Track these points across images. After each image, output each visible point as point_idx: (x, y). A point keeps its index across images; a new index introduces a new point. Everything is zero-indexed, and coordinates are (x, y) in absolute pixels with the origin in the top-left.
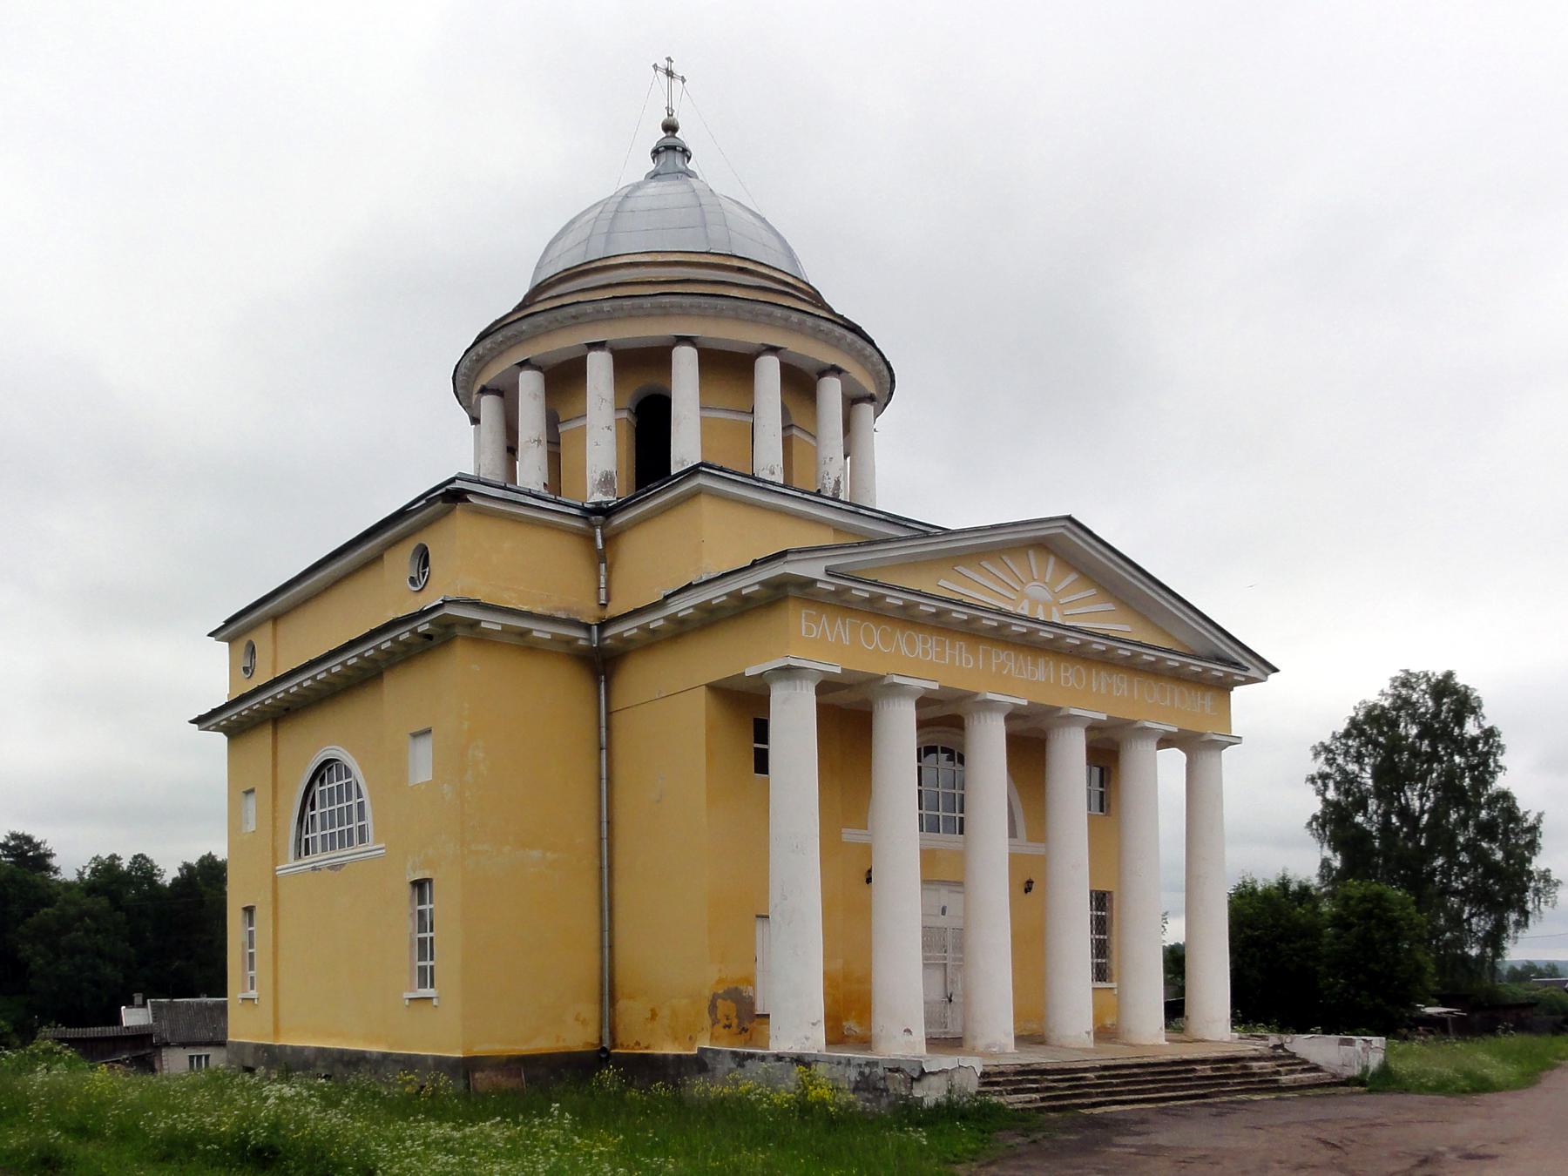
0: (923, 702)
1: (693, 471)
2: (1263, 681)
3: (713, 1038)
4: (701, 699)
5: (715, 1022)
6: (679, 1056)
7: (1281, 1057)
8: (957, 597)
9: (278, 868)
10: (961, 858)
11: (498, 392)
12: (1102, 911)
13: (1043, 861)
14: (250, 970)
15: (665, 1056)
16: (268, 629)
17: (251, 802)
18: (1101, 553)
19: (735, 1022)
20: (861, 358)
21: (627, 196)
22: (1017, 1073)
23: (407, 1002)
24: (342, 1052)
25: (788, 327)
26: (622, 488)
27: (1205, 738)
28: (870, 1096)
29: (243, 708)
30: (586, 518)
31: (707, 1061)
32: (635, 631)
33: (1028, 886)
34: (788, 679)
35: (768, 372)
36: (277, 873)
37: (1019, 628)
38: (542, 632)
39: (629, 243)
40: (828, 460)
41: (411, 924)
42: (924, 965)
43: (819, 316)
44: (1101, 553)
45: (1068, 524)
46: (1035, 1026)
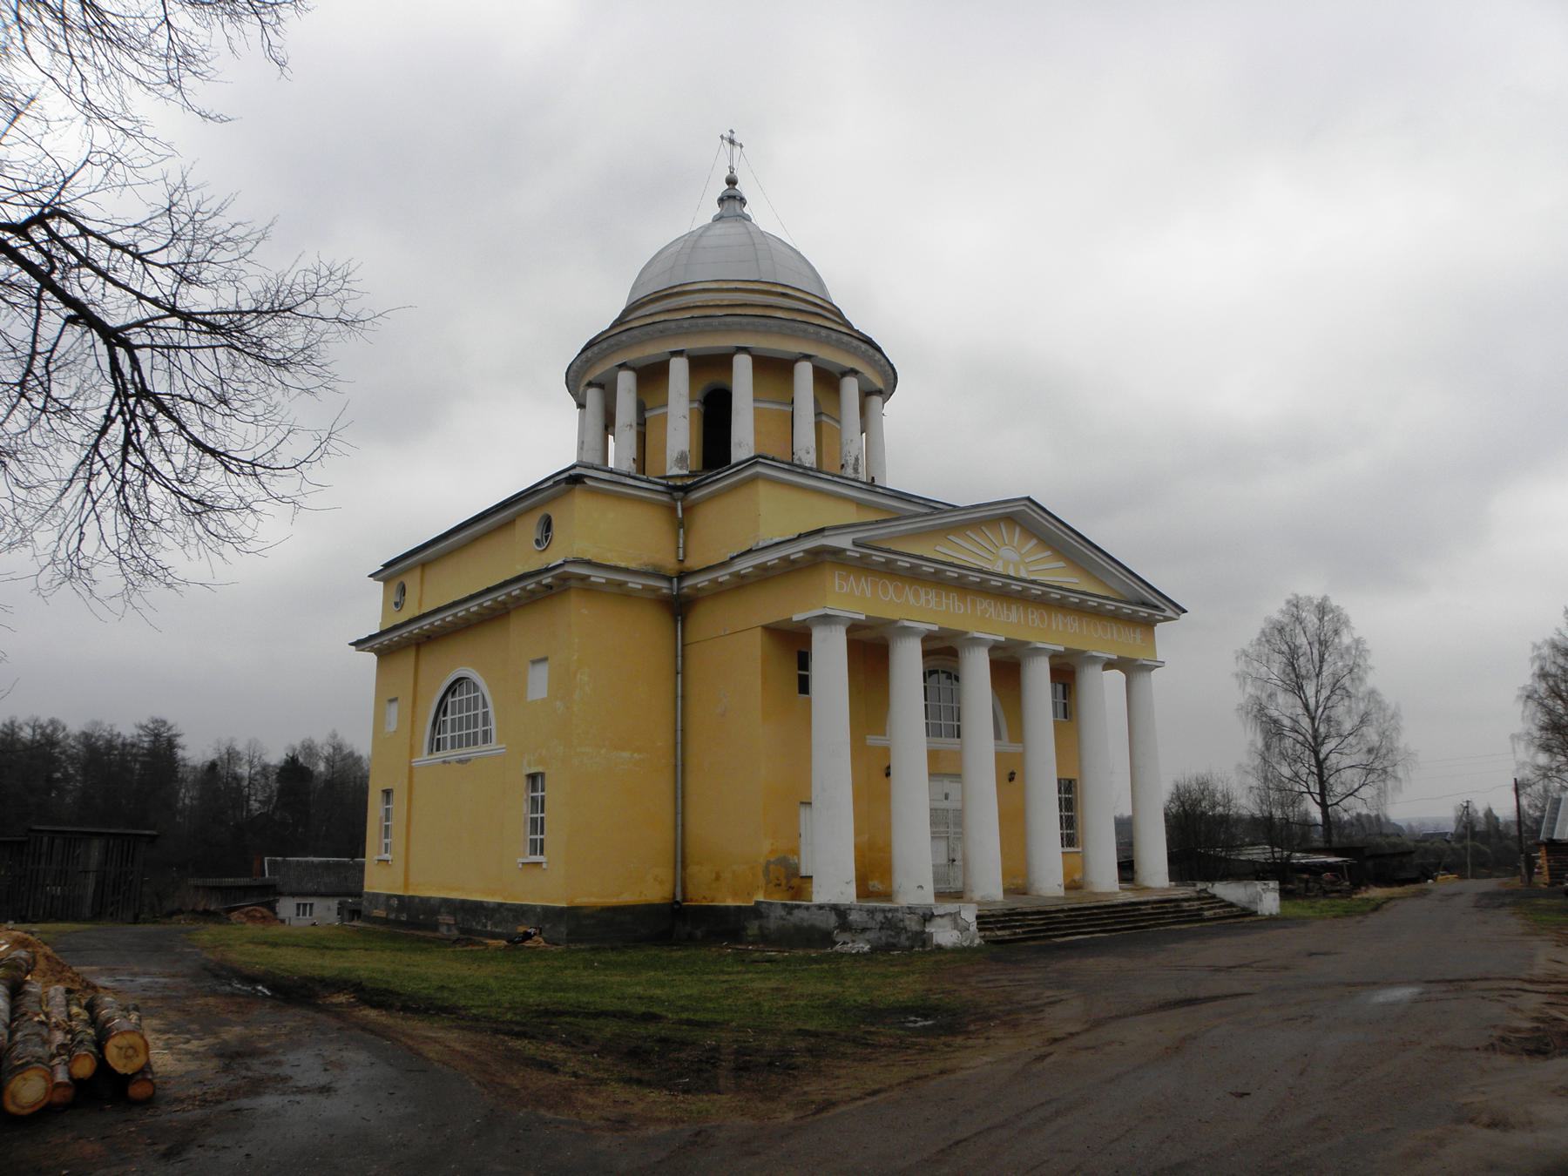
0: (928, 638)
1: (753, 461)
2: (1175, 619)
3: (766, 894)
4: (758, 633)
5: (768, 882)
6: (739, 907)
7: (1204, 898)
8: (950, 560)
9: (414, 760)
10: (958, 756)
11: (601, 386)
12: (1069, 794)
13: (1021, 758)
14: (385, 838)
15: (727, 908)
16: (417, 574)
17: (394, 708)
18: (1054, 525)
19: (784, 882)
20: (872, 362)
21: (701, 236)
22: (1005, 915)
23: (520, 866)
24: (463, 902)
25: (819, 341)
26: (695, 463)
27: (1139, 663)
28: (893, 933)
29: (395, 636)
30: (671, 494)
31: (763, 910)
32: (706, 583)
33: (1012, 777)
34: (826, 624)
36: (413, 764)
37: (996, 582)
38: (635, 583)
39: (704, 272)
40: (849, 442)
41: (525, 807)
42: (932, 837)
43: (840, 332)
44: (1054, 525)
45: (1027, 503)
46: (1020, 882)
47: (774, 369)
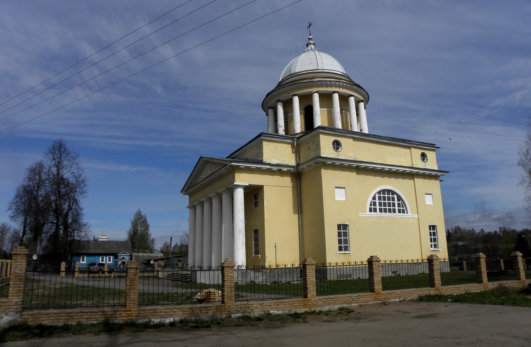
11: (272, 108)
35: (336, 97)
47: (326, 98)
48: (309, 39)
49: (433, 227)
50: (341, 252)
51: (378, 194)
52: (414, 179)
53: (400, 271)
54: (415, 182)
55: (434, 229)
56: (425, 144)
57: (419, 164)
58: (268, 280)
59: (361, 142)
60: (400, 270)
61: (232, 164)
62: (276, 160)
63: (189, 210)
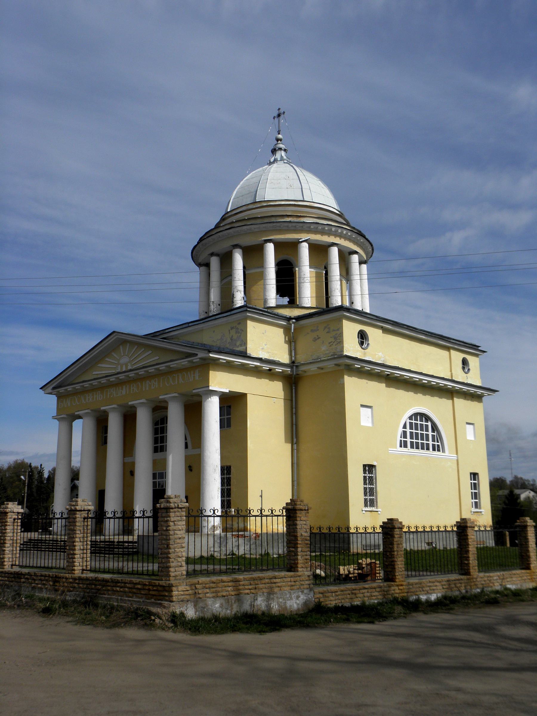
35: (334, 252)
48: (278, 140)
49: (474, 476)
50: (367, 509)
51: (409, 420)
52: (452, 399)
53: (436, 542)
54: (455, 405)
55: (370, 472)
56: (467, 345)
57: (460, 376)
58: (253, 551)
59: (401, 339)
60: (436, 540)
61: (211, 355)
62: (263, 353)
63: (56, 422)
